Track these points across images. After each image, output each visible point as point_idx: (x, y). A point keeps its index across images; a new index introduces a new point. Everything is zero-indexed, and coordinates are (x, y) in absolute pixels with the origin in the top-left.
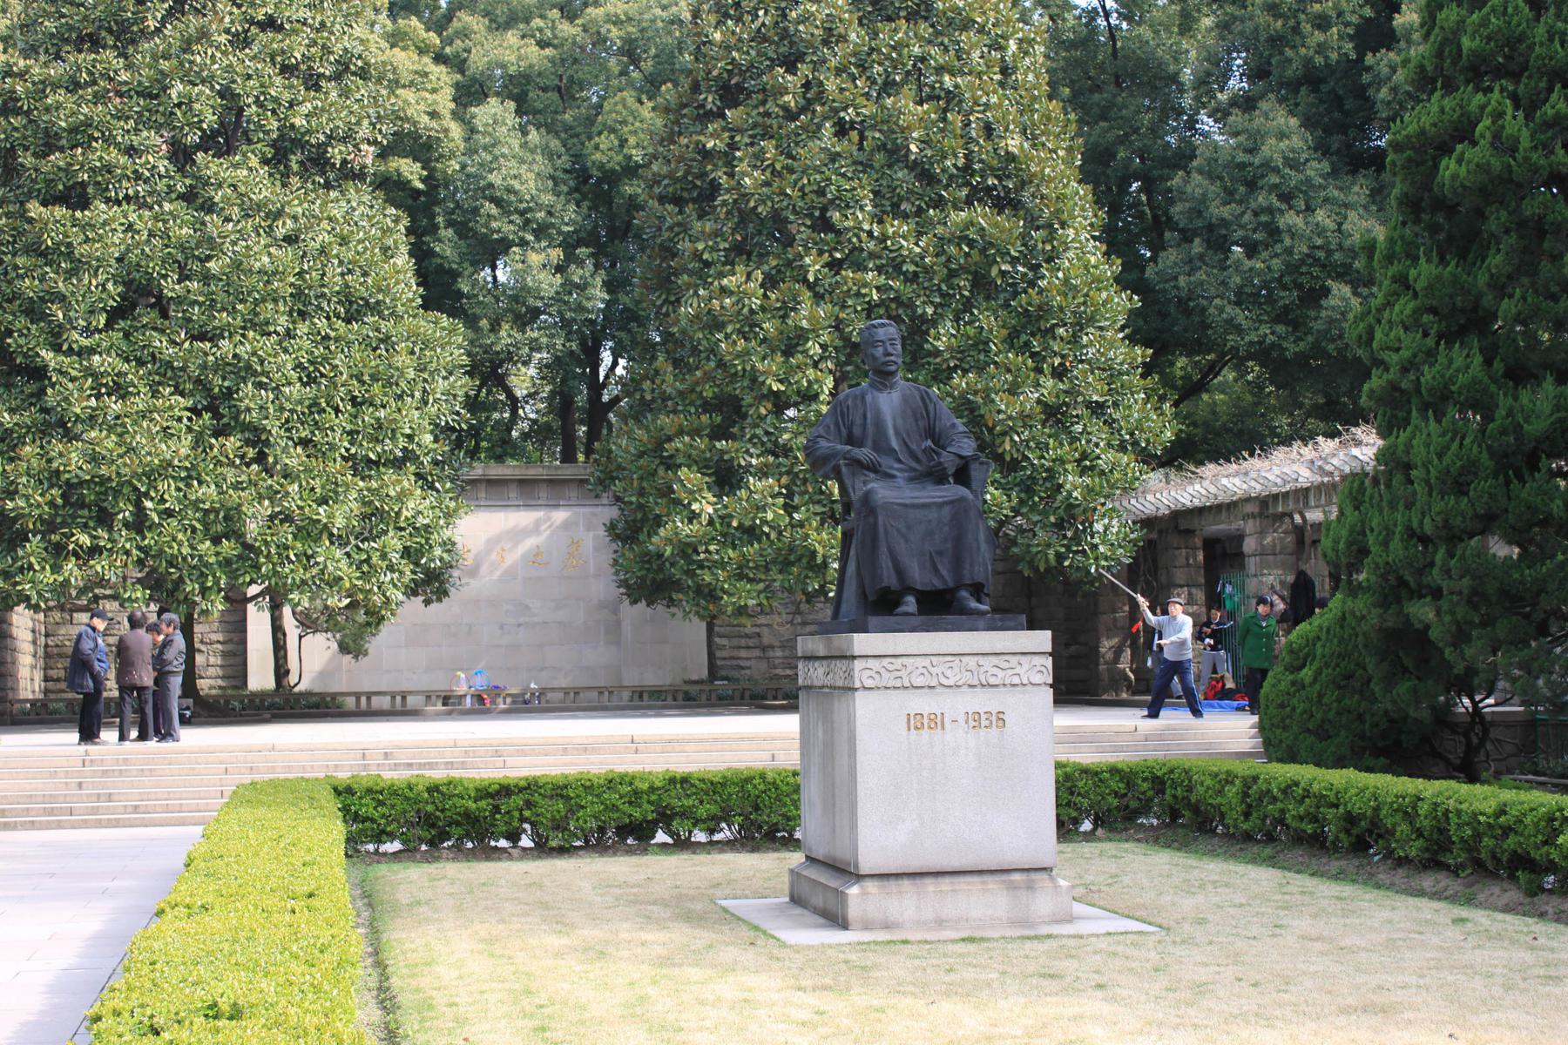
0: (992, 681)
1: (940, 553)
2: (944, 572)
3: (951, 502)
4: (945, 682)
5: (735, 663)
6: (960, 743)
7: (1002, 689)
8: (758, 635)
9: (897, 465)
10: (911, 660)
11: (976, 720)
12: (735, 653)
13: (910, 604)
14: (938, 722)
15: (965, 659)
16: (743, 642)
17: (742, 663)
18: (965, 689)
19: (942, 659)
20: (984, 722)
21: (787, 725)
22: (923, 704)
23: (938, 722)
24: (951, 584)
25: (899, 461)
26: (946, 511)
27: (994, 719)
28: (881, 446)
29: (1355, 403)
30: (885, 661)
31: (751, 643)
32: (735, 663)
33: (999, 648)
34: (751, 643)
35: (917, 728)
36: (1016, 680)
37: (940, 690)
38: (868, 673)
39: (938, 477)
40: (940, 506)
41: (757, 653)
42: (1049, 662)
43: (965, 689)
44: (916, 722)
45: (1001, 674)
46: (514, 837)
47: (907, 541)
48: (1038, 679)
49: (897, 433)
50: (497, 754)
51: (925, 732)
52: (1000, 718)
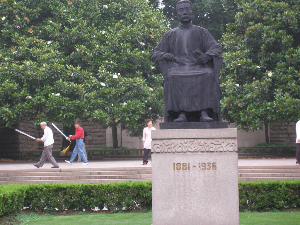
0: (211, 150)
1: (196, 96)
2: (197, 104)
3: (202, 75)
4: (190, 150)
5: (278, 139)
6: (197, 176)
7: (215, 153)
8: (287, 129)
9: (187, 60)
10: (176, 141)
11: (203, 166)
12: (278, 136)
13: (182, 117)
14: (186, 167)
15: (199, 140)
16: (281, 132)
17: (281, 139)
18: (199, 153)
19: (189, 140)
20: (207, 167)
21: (239, 165)
22: (180, 159)
23: (186, 167)
24: (199, 109)
25: (188, 58)
26: (199, 79)
27: (211, 165)
28: (180, 53)
29: (257, 31)
30: (164, 141)
31: (284, 132)
32: (278, 139)
33: (214, 135)
34: (284, 132)
35: (178, 169)
36: (221, 149)
37: (188, 153)
38: (157, 146)
39: (201, 64)
40: (197, 76)
41: (286, 136)
42: (236, 142)
43: (199, 153)
44: (177, 167)
45: (214, 147)
46: (101, 207)
47: (182, 91)
48: (231, 149)
49: (188, 47)
50: (139, 173)
51: (181, 171)
52: (214, 165)
